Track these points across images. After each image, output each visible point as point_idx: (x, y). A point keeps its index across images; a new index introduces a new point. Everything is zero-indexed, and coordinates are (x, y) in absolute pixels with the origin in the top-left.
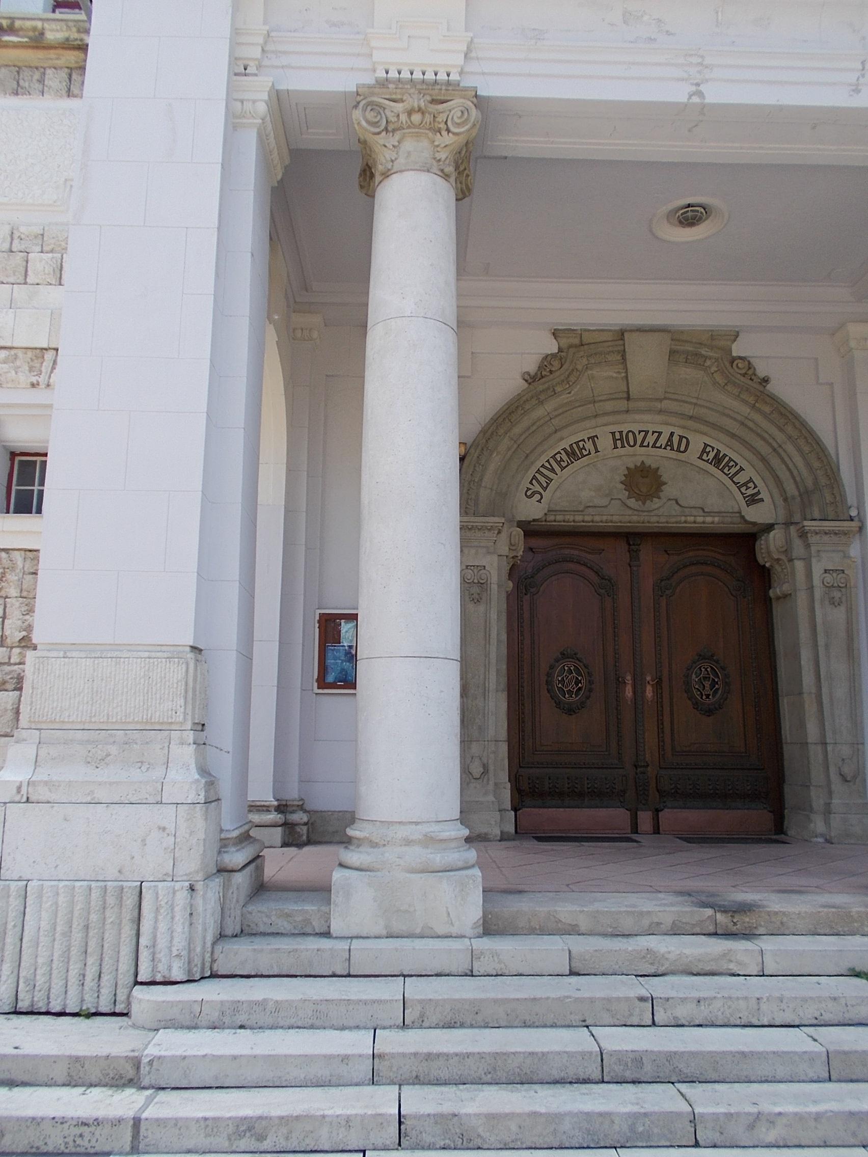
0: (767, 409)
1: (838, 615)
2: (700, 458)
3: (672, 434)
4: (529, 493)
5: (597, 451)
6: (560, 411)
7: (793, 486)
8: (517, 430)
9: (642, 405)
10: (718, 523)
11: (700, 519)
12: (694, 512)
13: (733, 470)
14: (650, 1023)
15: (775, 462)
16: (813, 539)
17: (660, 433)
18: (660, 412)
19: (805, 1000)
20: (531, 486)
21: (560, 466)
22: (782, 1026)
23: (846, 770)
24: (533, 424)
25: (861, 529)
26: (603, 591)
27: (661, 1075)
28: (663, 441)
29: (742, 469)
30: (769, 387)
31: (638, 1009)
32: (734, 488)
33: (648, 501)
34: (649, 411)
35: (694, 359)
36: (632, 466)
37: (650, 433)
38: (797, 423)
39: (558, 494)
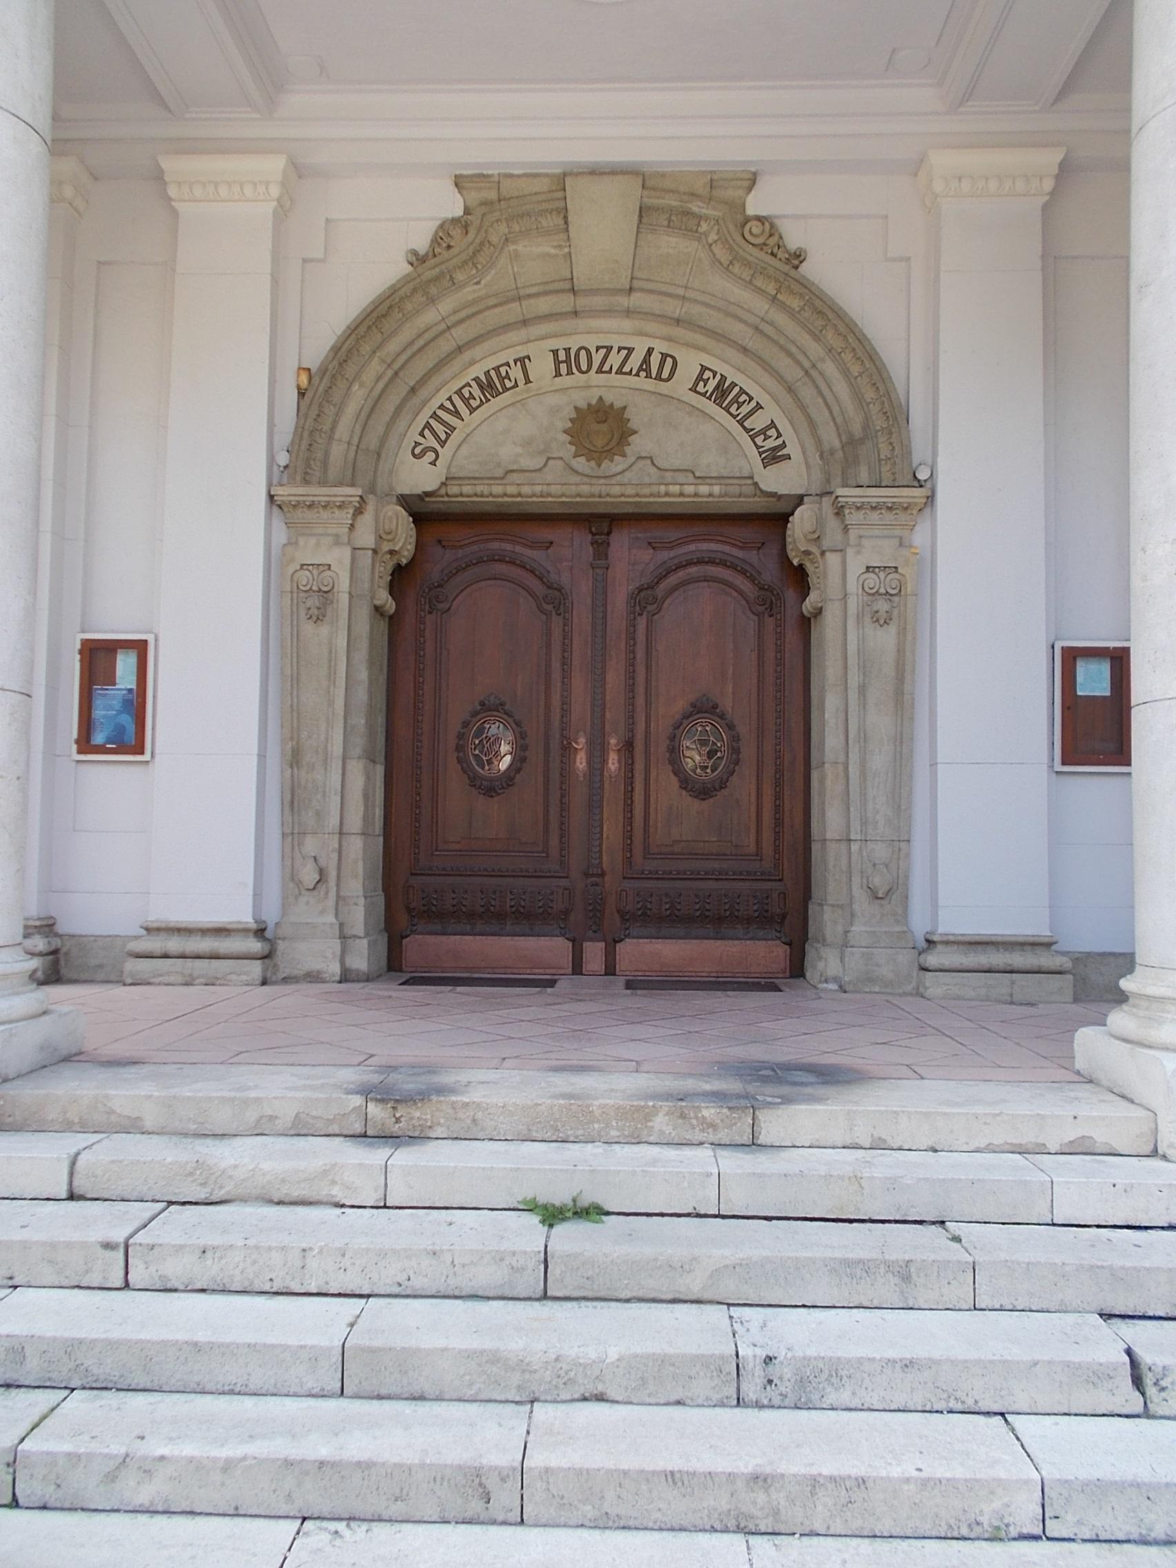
0: (795, 303)
1: (885, 639)
2: (694, 389)
3: (650, 351)
4: (417, 451)
5: (528, 381)
6: (463, 314)
7: (834, 434)
8: (393, 346)
9: (599, 301)
10: (720, 496)
11: (690, 489)
12: (681, 478)
13: (745, 409)
14: (119, 1283)
15: (807, 393)
16: (852, 517)
17: (630, 350)
18: (628, 313)
19: (383, 1254)
20: (421, 440)
21: (468, 405)
22: (339, 1295)
23: (877, 881)
24: (420, 336)
25: (931, 499)
26: (550, 607)
27: (54, 1375)
28: (635, 361)
29: (759, 407)
30: (804, 268)
31: (100, 1262)
32: (745, 438)
34: (608, 312)
35: (683, 220)
36: (582, 404)
37: (615, 350)
38: (841, 328)
39: (464, 450)
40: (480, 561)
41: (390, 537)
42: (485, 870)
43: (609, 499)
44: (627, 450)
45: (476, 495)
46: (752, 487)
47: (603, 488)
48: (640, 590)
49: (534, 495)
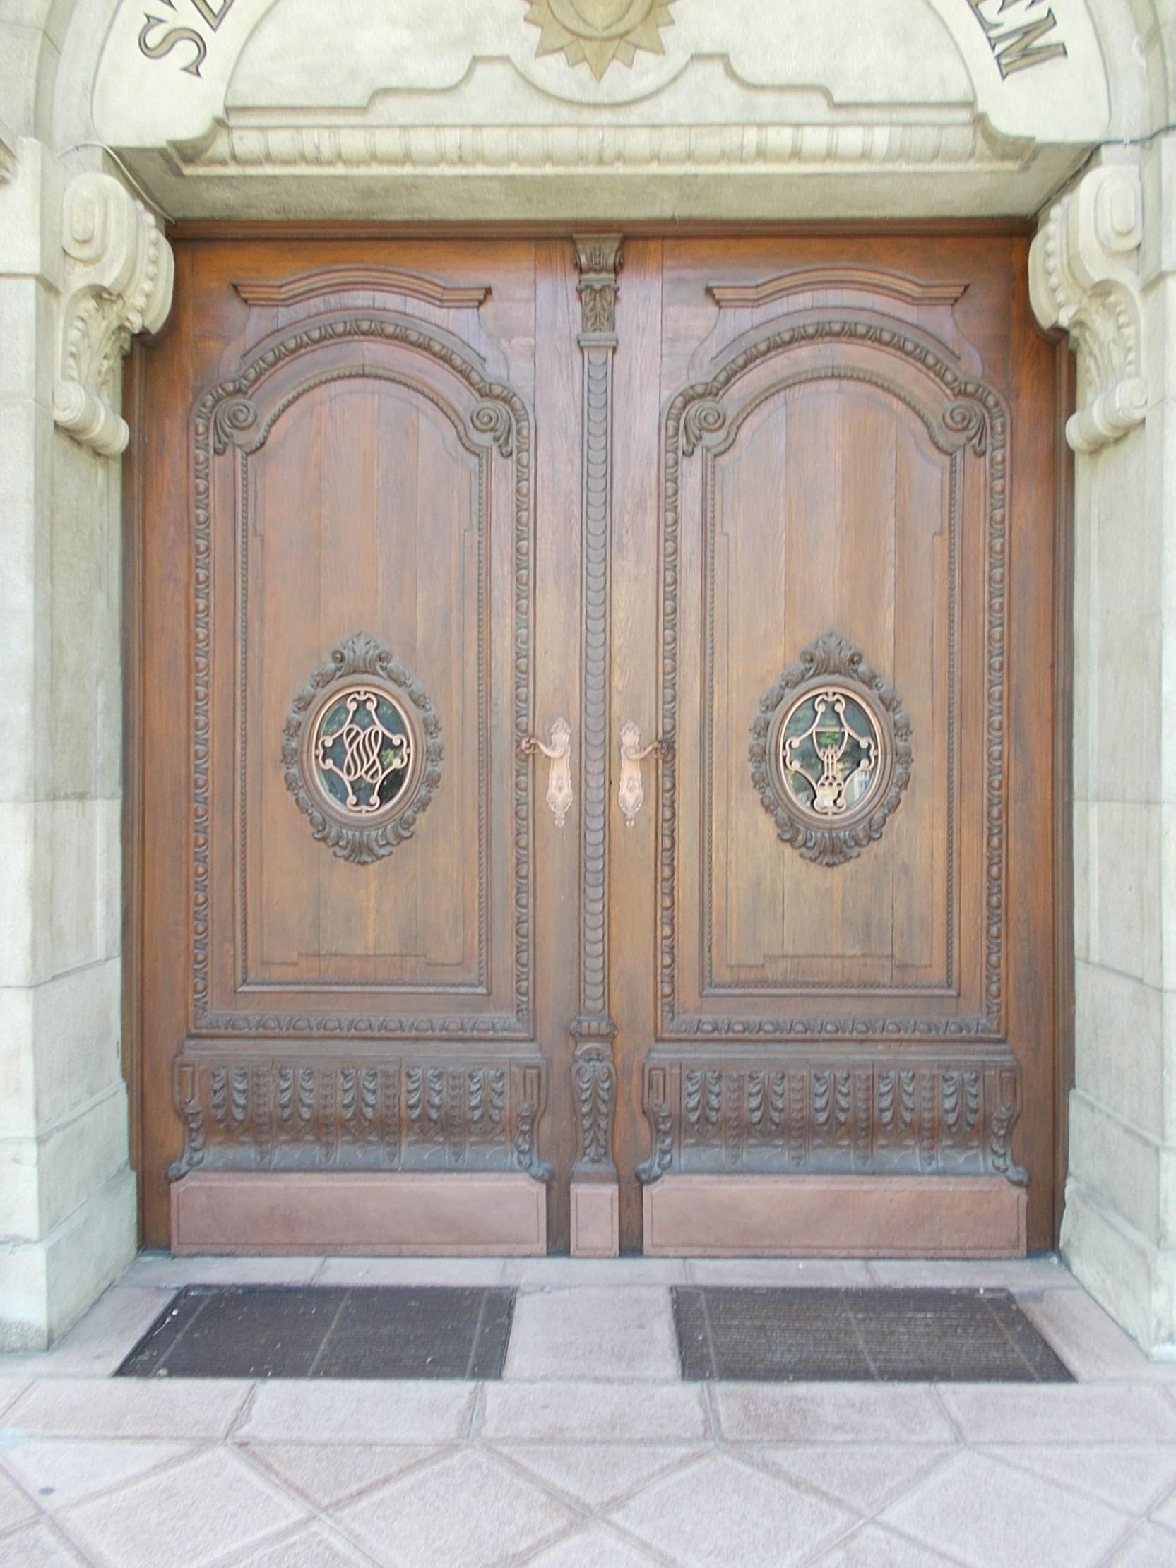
10: (887, 158)
11: (815, 139)
12: (796, 106)
20: (162, 11)
26: (486, 439)
33: (616, 66)
39: (269, 38)
40: (328, 337)
41: (86, 252)
42: (353, 1025)
43: (621, 169)
44: (668, 36)
45: (304, 159)
46: (967, 132)
47: (609, 135)
48: (689, 398)
49: (441, 159)
